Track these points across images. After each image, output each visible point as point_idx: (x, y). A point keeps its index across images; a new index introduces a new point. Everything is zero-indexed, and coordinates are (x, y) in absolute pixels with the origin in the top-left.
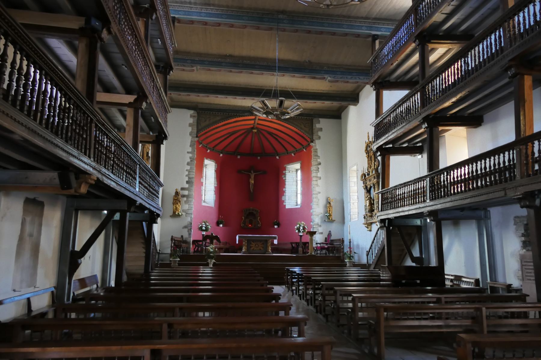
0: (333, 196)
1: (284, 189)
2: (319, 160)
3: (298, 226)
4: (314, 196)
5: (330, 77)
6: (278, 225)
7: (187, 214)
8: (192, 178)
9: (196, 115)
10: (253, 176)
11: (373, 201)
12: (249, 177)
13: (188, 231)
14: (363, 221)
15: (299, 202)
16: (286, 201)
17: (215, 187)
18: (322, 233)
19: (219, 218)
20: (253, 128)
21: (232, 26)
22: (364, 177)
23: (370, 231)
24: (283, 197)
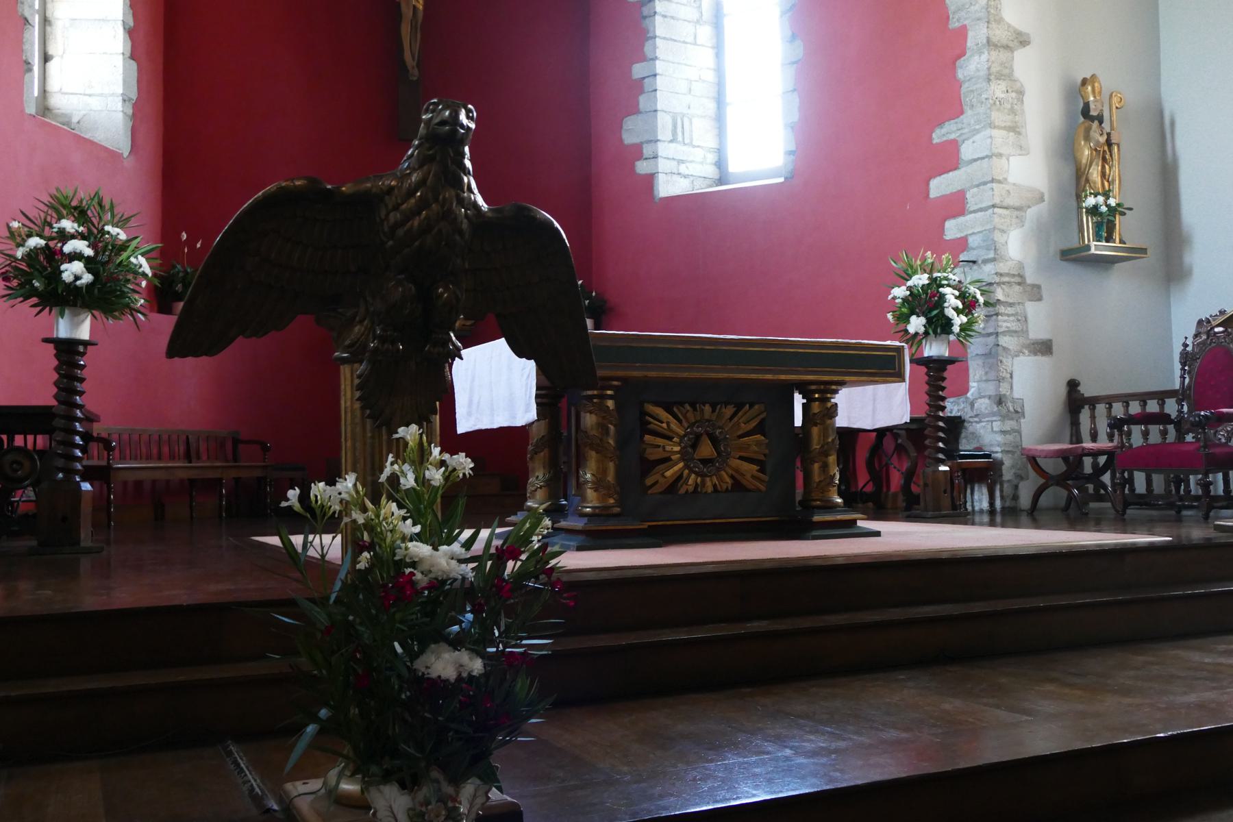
16: (664, 149)
18: (1044, 348)
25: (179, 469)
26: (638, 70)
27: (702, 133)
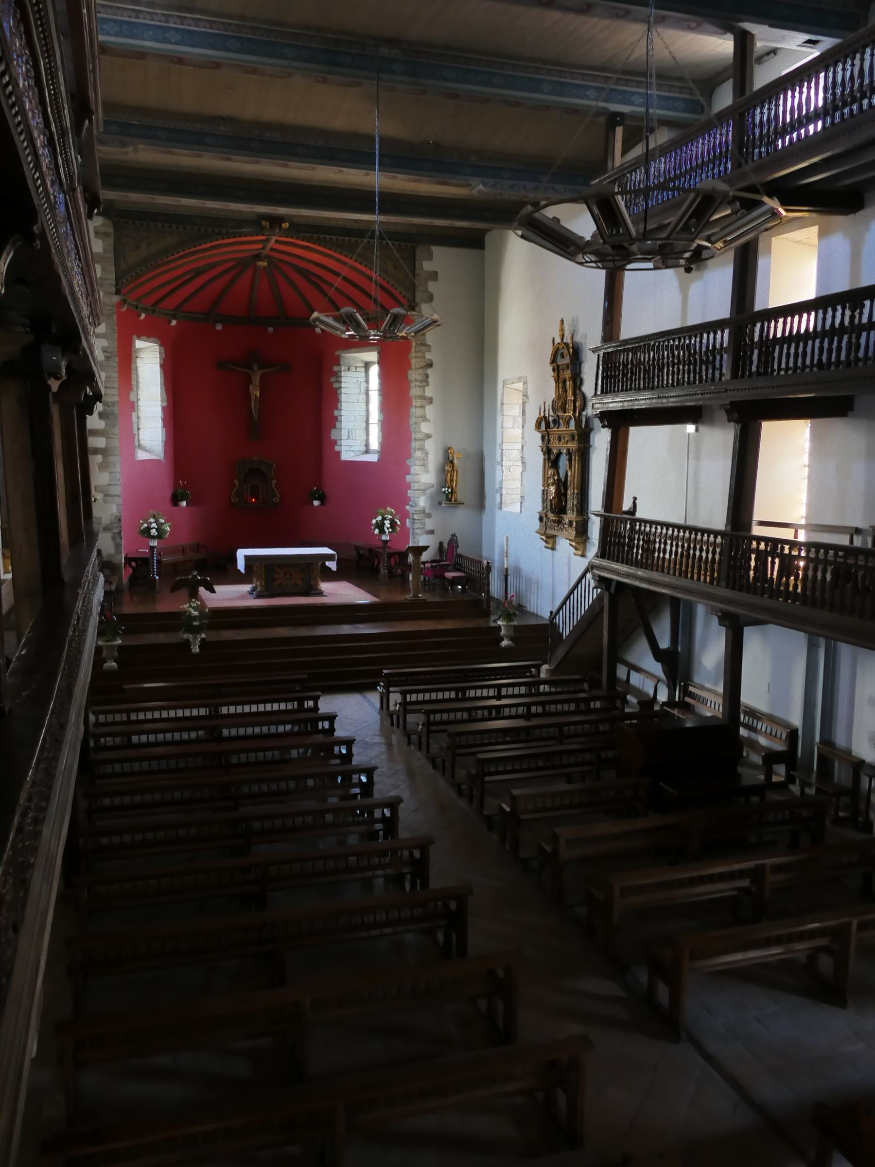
0: (460, 444)
1: (336, 413)
2: (428, 356)
3: (379, 518)
4: (414, 444)
5: (484, 184)
6: (322, 498)
7: (106, 495)
8: (113, 404)
9: (110, 230)
10: (256, 379)
11: (566, 489)
12: (249, 381)
13: (114, 539)
14: (537, 524)
15: (375, 443)
16: (343, 443)
17: (164, 409)
18: (432, 532)
19: (176, 484)
20: (258, 257)
21: (254, 71)
22: (545, 425)
23: (553, 549)
24: (333, 431)
25: (179, 557)
26: (336, 413)
27: (360, 435)
